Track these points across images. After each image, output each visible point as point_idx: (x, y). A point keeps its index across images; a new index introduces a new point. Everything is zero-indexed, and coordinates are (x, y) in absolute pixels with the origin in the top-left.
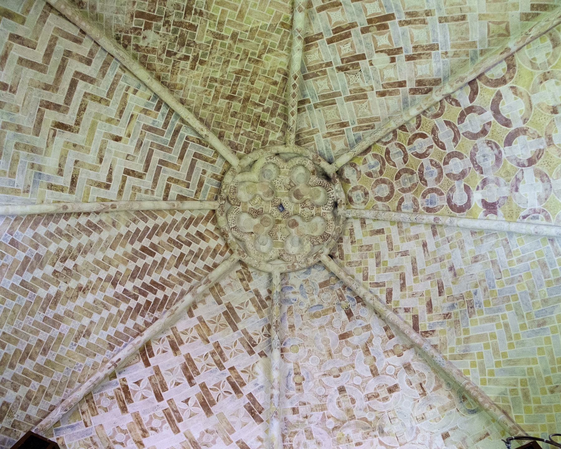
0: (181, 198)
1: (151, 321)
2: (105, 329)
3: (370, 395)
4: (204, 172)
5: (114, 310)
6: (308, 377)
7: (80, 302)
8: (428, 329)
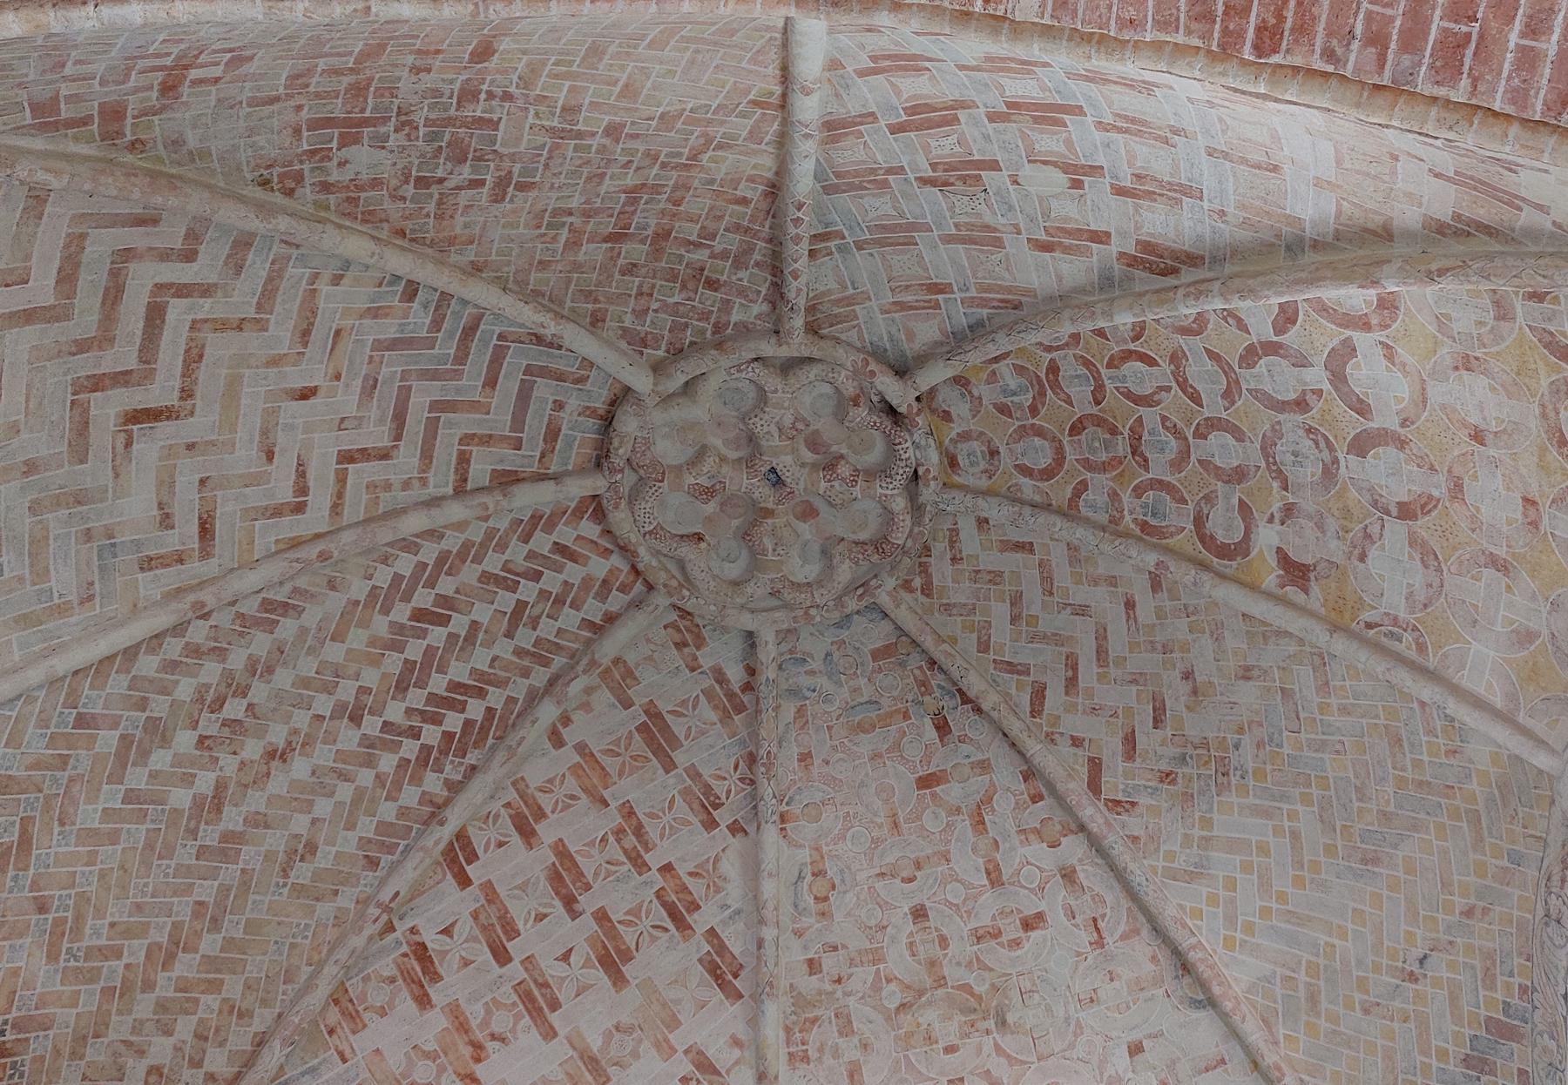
0: (506, 480)
1: (460, 778)
2: (351, 826)
3: (981, 932)
4: (559, 405)
5: (366, 777)
6: (843, 881)
7: (278, 784)
8: (1120, 797)
